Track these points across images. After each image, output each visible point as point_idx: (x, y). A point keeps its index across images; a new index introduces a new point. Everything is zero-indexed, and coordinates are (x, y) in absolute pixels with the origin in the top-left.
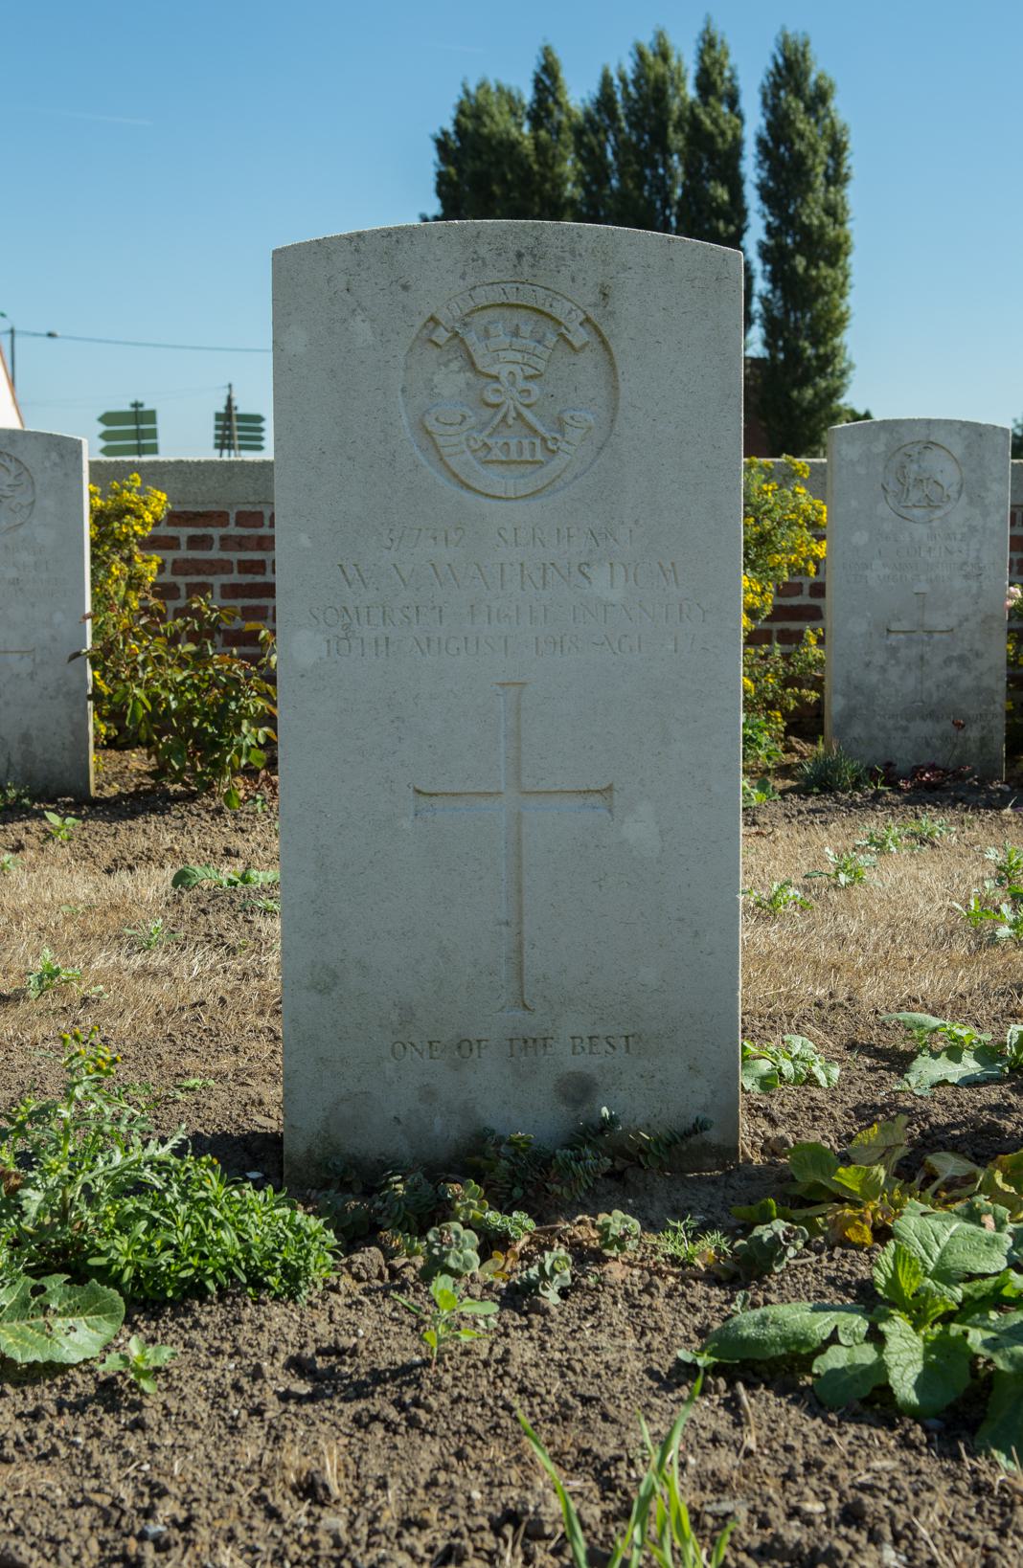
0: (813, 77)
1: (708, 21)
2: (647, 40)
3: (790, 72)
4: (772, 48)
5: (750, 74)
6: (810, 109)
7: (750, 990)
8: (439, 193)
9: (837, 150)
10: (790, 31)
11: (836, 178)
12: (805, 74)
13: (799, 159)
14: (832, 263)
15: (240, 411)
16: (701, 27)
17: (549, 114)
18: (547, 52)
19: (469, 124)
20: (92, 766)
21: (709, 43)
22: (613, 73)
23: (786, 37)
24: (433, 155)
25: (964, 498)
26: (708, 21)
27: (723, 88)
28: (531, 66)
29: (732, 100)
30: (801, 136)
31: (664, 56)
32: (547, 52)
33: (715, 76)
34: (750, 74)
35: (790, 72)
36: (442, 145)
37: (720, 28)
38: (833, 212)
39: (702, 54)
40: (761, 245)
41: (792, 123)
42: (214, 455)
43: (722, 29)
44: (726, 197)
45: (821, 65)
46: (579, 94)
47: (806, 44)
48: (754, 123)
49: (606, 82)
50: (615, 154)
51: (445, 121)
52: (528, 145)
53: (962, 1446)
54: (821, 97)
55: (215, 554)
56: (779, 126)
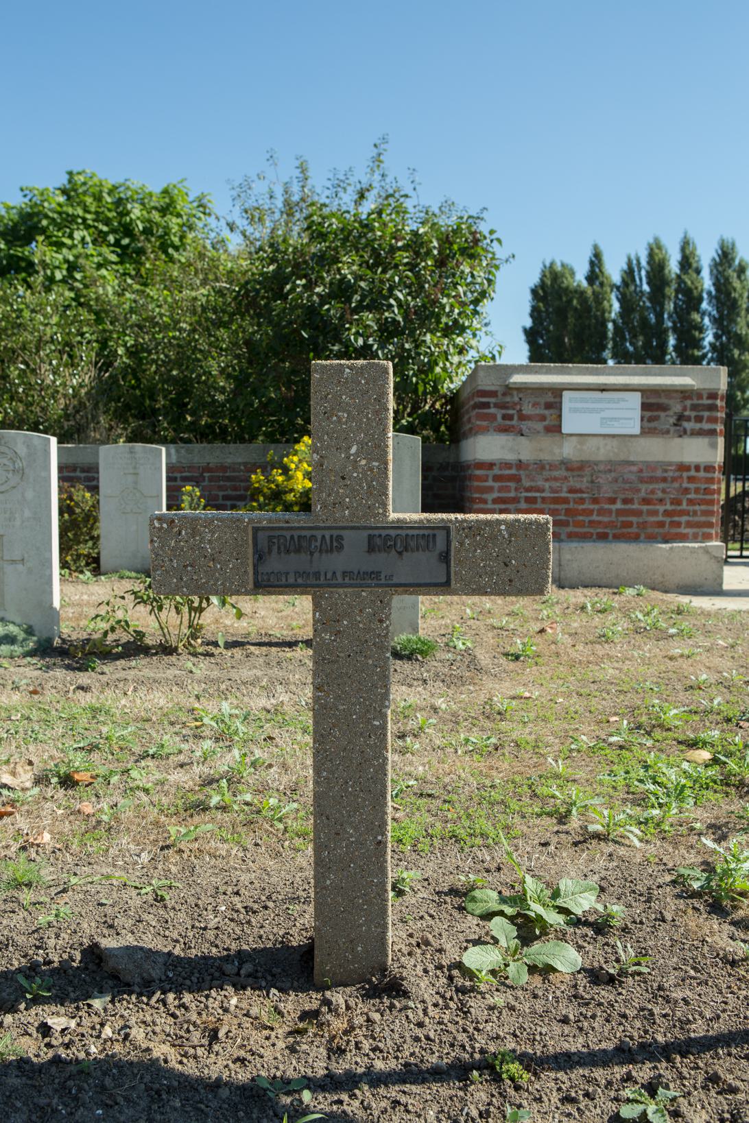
0: (737, 262)
1: (686, 233)
3: (725, 256)
4: (717, 246)
5: (706, 256)
6: (739, 277)
8: (532, 316)
10: (725, 237)
12: (733, 259)
13: (735, 301)
15: (66, 182)
16: (682, 235)
17: (597, 277)
18: (596, 247)
19: (549, 282)
22: (633, 257)
23: (723, 241)
24: (529, 296)
25: (164, 978)
26: (686, 233)
27: (694, 265)
28: (588, 254)
29: (698, 271)
30: (735, 290)
31: (659, 248)
32: (596, 247)
33: (691, 260)
34: (706, 256)
35: (725, 256)
39: (683, 249)
40: (710, 344)
41: (730, 283)
42: (417, 516)
43: (692, 235)
44: (653, 320)
46: (614, 272)
47: (733, 245)
48: (707, 282)
49: (629, 263)
50: (670, 316)
51: (534, 279)
52: (589, 292)
55: (635, 506)
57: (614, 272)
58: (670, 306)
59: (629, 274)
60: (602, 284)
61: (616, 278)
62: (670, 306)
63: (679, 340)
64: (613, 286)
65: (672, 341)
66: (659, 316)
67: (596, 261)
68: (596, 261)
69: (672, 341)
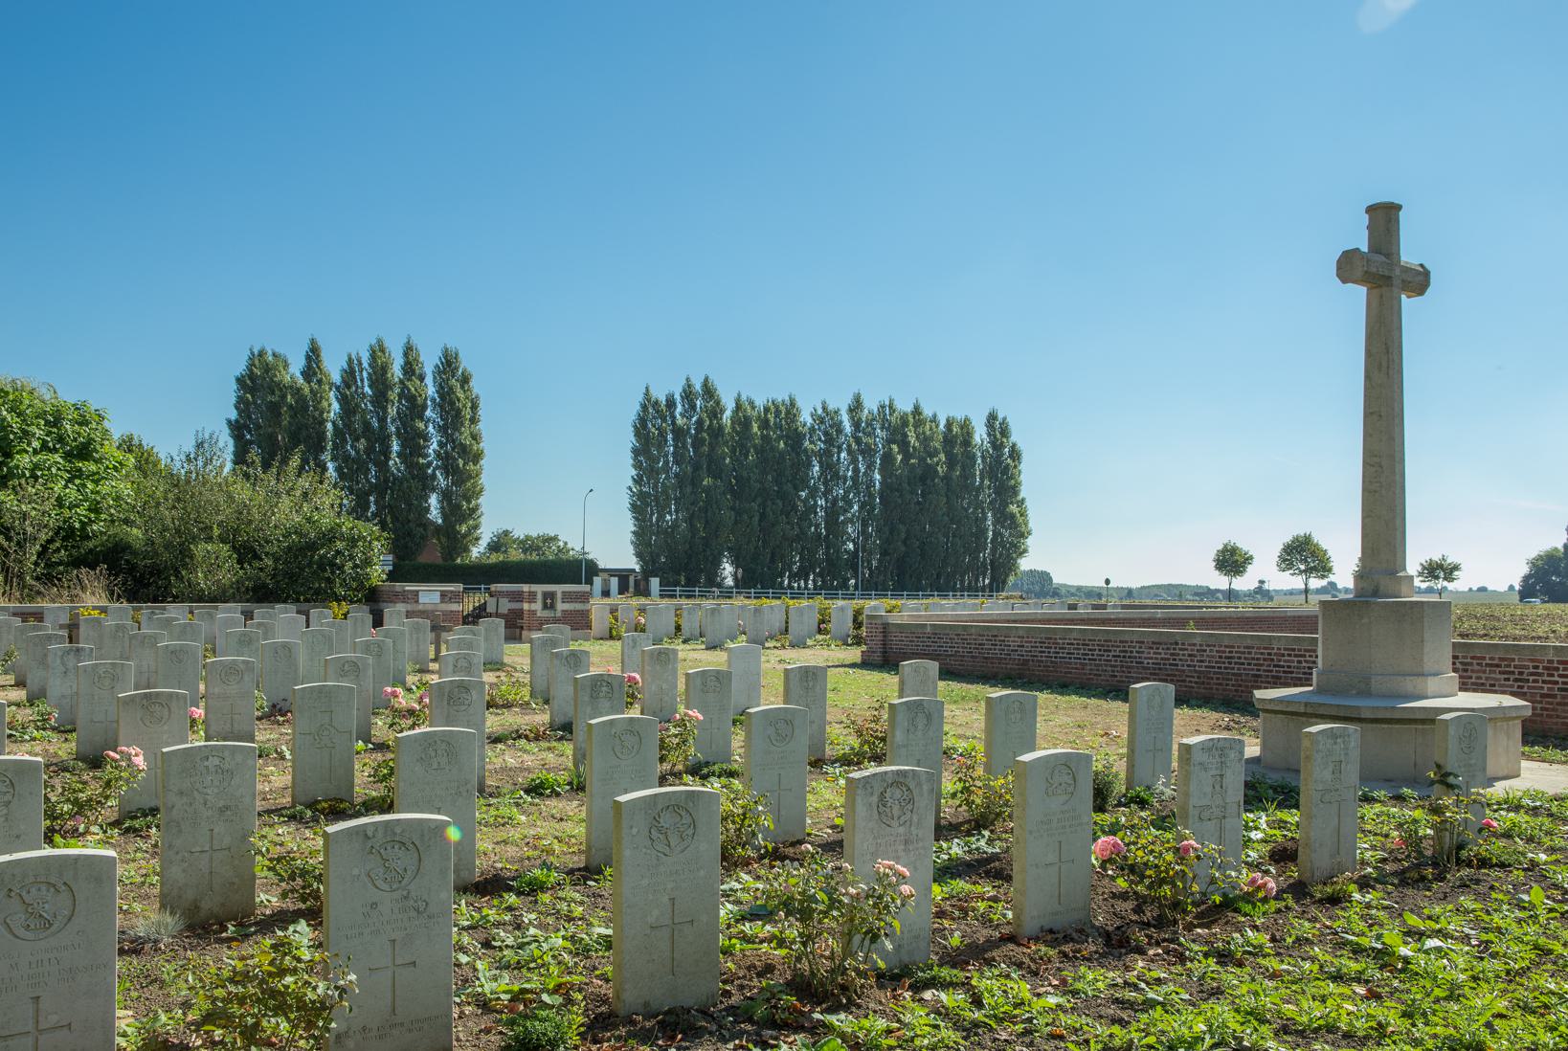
2: (374, 342)
3: (449, 364)
5: (429, 362)
7: (828, 718)
9: (474, 407)
11: (474, 420)
14: (476, 462)
16: (641, 398)
18: (313, 341)
20: (27, 757)
21: (408, 350)
28: (306, 347)
32: (313, 341)
35: (449, 364)
36: (240, 381)
37: (415, 341)
38: (475, 437)
39: (406, 355)
45: (465, 363)
46: (333, 368)
49: (350, 361)
51: (240, 367)
53: (1027, 757)
54: (465, 380)
56: (446, 395)
57: (333, 368)
58: (392, 411)
59: (350, 375)
60: (320, 382)
61: (336, 377)
62: (392, 411)
63: (403, 446)
64: (331, 385)
65: (395, 447)
66: (382, 420)
67: (314, 354)
68: (314, 354)
69: (395, 447)
